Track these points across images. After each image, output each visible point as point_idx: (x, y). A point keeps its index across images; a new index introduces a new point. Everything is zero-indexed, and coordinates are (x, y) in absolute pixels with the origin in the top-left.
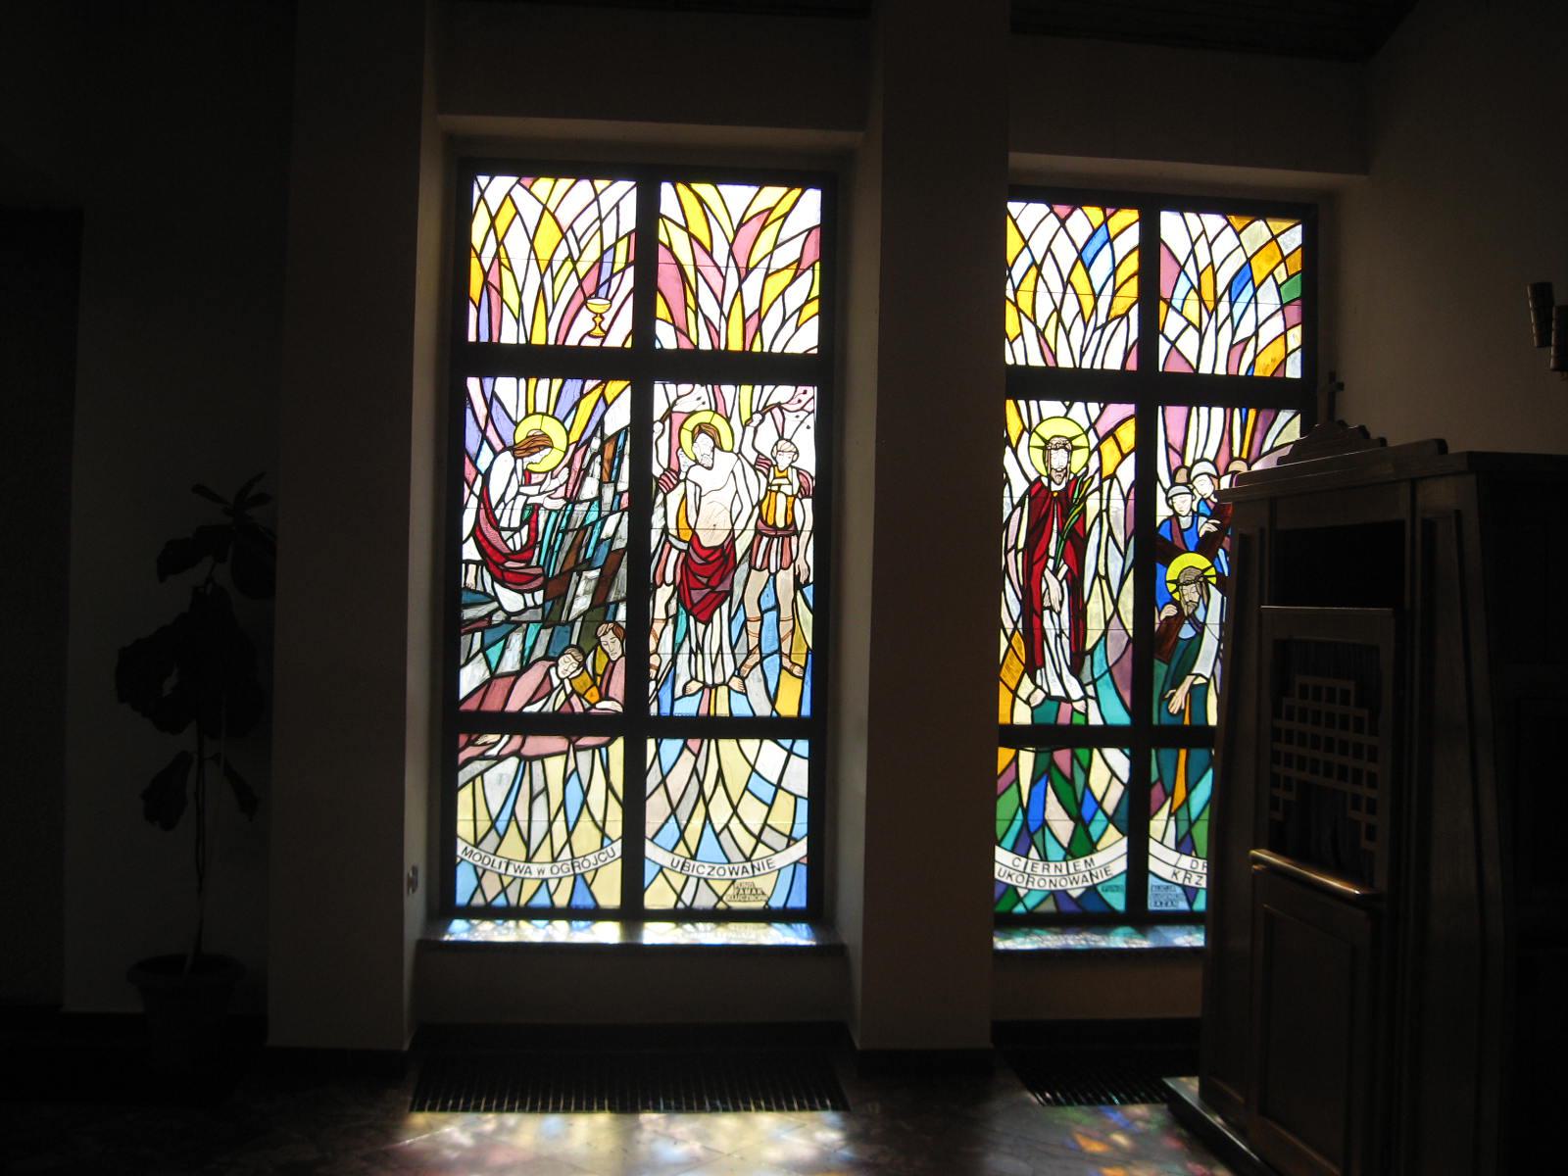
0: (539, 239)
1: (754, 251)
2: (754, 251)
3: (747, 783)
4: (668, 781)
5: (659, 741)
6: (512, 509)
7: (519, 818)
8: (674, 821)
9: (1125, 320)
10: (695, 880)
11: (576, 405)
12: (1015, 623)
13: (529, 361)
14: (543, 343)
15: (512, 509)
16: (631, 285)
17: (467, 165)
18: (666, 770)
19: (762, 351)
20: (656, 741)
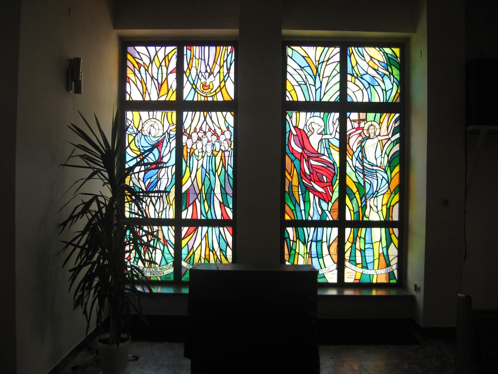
0: (151, 68)
1: (214, 70)
2: (214, 70)
3: (196, 126)
4: (155, 53)
5: (200, 262)
6: (168, 179)
7: (157, 213)
8: (160, 61)
9: (158, 212)
10: (322, 268)
11: (219, 244)
12: (172, 176)
13: (343, 63)
14: (382, 228)
15: (168, 179)
16: (174, 182)
17: (88, 209)
18: (205, 169)
19: (204, 100)
20: (166, 190)
